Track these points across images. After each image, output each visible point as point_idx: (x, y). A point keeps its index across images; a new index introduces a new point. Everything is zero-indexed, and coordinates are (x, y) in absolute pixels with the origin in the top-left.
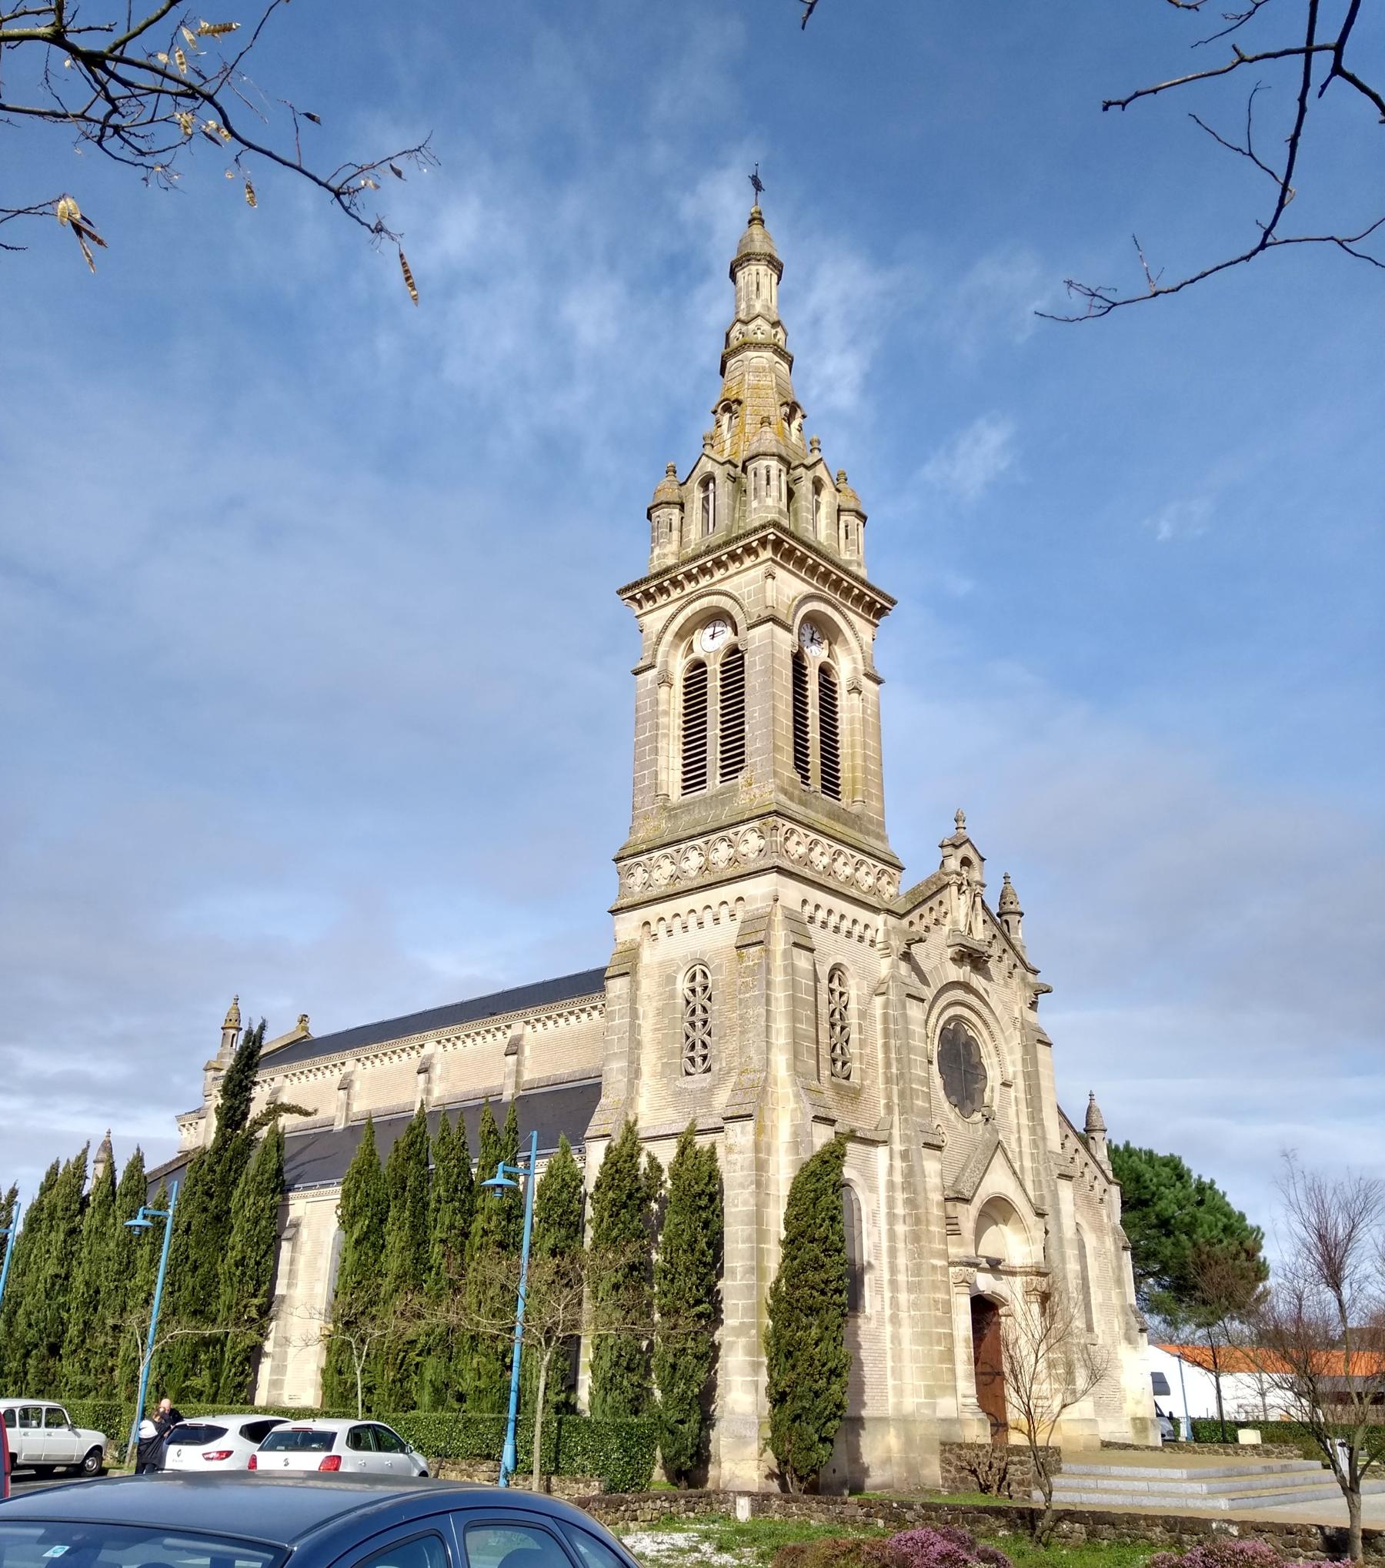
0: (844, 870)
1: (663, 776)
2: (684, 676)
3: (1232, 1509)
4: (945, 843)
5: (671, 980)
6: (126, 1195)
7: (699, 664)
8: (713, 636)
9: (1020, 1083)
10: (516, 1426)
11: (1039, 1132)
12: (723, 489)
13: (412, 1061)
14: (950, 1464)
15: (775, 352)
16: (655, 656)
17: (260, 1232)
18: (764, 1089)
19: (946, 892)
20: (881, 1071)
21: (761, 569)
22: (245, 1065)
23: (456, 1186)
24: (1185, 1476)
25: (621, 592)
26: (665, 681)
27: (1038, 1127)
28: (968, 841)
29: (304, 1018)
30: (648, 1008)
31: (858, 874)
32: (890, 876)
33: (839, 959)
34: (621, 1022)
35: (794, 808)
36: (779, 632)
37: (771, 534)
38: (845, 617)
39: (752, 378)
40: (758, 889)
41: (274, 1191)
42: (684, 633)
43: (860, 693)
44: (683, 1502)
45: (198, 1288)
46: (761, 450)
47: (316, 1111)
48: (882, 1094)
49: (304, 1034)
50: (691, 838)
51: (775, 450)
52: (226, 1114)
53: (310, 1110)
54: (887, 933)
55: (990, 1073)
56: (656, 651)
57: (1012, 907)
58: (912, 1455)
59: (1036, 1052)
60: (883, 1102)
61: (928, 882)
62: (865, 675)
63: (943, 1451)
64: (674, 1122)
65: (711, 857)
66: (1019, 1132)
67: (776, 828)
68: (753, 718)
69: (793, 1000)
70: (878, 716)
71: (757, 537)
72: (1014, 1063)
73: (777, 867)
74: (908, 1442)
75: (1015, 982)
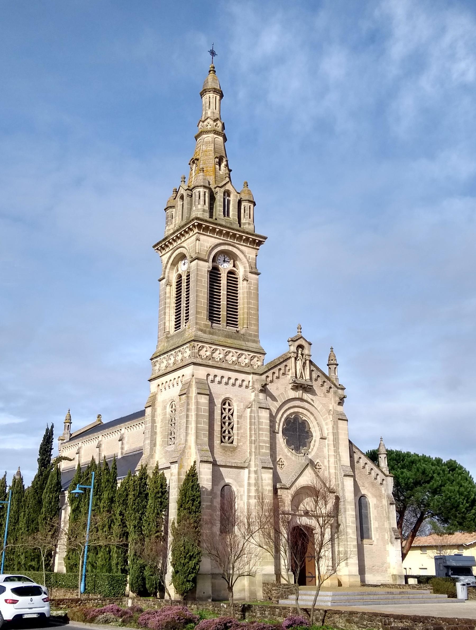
0: (231, 358)
1: (167, 324)
2: (176, 281)
3: (332, 606)
4: (289, 340)
5: (165, 408)
6: (16, 493)
7: (180, 276)
8: (184, 264)
9: (331, 437)
10: (85, 577)
11: (338, 458)
12: (186, 199)
13: (117, 436)
14: (265, 591)
15: (215, 133)
16: (164, 274)
17: (52, 507)
18: (184, 451)
19: (289, 361)
20: (248, 438)
21: (194, 238)
22: (46, 443)
23: (98, 490)
24: (332, 595)
25: (154, 247)
26: (169, 284)
27: (338, 456)
28: (301, 337)
29: (99, 416)
30: (158, 419)
31: (240, 360)
32: (258, 358)
33: (227, 396)
34: (149, 425)
35: (206, 337)
36: (201, 263)
37: (196, 222)
38: (239, 249)
39: (204, 147)
40: (188, 371)
41: (57, 491)
42: (175, 264)
43: (247, 281)
44: (108, 601)
45: (34, 528)
46: (197, 184)
47: (74, 458)
48: (248, 448)
49: (99, 422)
50: (171, 351)
51: (202, 184)
52: (41, 462)
53: (72, 459)
54: (253, 382)
55: (314, 434)
56: (165, 271)
57: (332, 362)
58: (252, 588)
59: (337, 424)
60: (249, 451)
61: (279, 359)
62: (250, 272)
63: (263, 586)
64: (165, 463)
65: (176, 358)
66: (328, 458)
67: (194, 347)
68: (191, 300)
69: (197, 416)
70: (257, 289)
71: (191, 224)
72: (328, 429)
73: (192, 363)
74: (252, 583)
75: (331, 394)
